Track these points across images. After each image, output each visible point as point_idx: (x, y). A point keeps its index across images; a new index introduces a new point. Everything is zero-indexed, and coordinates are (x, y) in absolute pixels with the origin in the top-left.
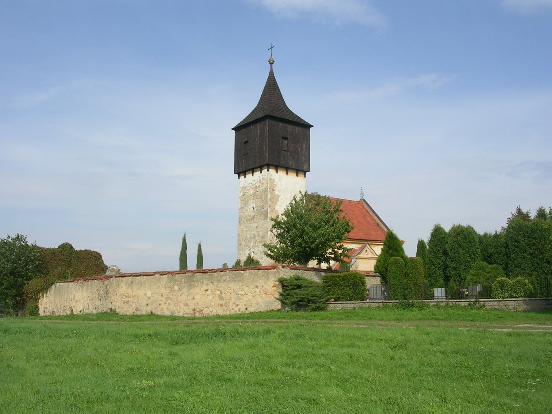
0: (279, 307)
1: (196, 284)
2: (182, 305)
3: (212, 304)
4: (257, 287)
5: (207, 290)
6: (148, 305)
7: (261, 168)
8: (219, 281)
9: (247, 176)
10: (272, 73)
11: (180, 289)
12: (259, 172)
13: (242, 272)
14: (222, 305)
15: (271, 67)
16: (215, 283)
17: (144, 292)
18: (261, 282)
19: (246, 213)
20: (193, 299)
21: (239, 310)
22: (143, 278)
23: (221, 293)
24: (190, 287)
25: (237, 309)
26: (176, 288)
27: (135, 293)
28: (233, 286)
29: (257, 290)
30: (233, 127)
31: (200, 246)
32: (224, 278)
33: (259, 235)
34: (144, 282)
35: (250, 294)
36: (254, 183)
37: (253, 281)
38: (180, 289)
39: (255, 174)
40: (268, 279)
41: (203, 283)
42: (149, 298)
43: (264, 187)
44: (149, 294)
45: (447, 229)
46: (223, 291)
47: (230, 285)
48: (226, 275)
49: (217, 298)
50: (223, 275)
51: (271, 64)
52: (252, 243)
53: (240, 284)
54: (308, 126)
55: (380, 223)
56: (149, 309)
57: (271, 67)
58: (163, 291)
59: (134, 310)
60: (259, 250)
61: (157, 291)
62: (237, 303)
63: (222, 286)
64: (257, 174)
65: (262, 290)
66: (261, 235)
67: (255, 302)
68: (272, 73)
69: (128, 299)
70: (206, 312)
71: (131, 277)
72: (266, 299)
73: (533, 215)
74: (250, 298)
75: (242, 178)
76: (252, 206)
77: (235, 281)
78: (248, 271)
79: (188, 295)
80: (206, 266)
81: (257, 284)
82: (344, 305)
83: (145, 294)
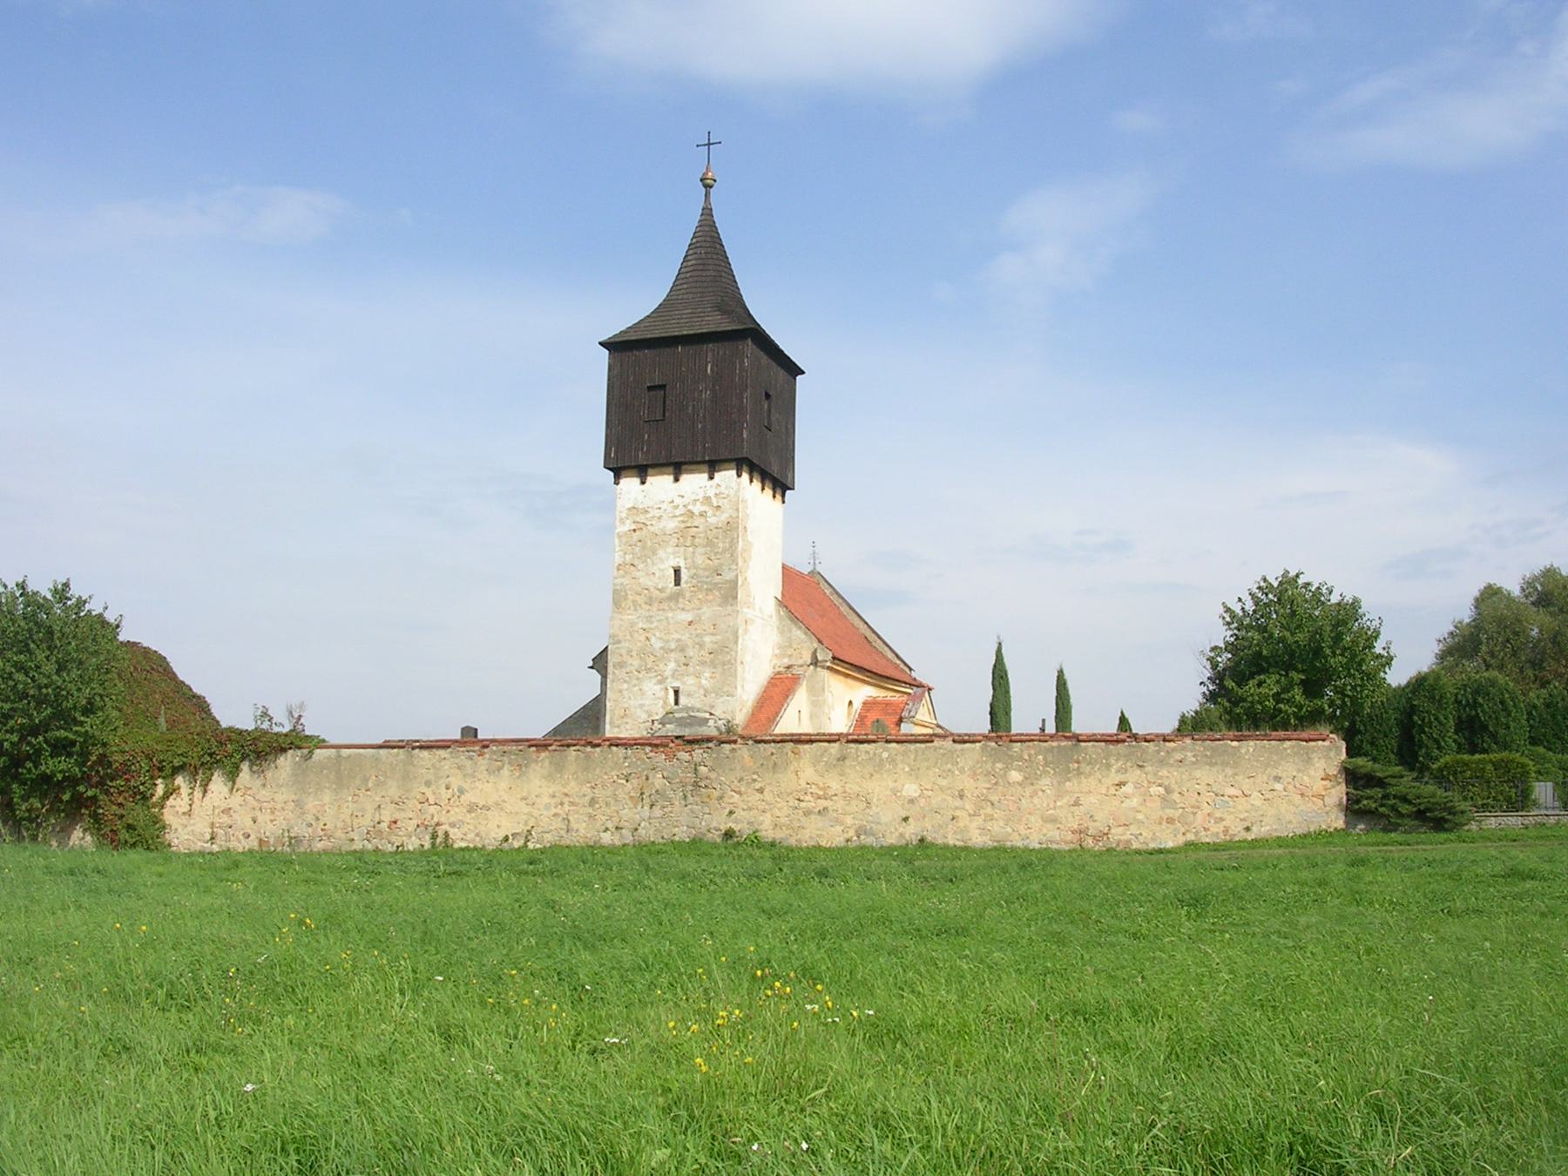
0: (1340, 823)
1: (1086, 768)
2: (1035, 821)
3: (1140, 816)
4: (1277, 779)
5: (1121, 784)
6: (906, 819)
7: (713, 466)
8: (1162, 763)
9: (649, 479)
10: (707, 212)
11: (1029, 780)
12: (706, 476)
13: (1235, 744)
14: (1170, 821)
15: (707, 195)
16: (1149, 769)
17: (891, 785)
18: (1288, 769)
19: (645, 581)
20: (1077, 804)
21: (1226, 831)
22: (885, 750)
23: (1168, 790)
24: (1065, 775)
25: (1218, 829)
26: (1015, 776)
27: (853, 788)
28: (1205, 775)
29: (1278, 786)
30: (604, 338)
31: (1000, 676)
32: (1178, 756)
33: (701, 645)
34: (892, 761)
35: (1256, 794)
36: (678, 501)
37: (1268, 765)
38: (1029, 780)
39: (685, 478)
40: (1308, 761)
41: (1108, 766)
42: (911, 801)
43: (724, 517)
44: (911, 789)
45: (123, 637)
46: (1174, 786)
47: (1198, 774)
48: (1184, 749)
49: (1157, 803)
50: (1174, 750)
51: (708, 187)
52: (672, 665)
53: (1229, 771)
54: (794, 371)
55: (872, 637)
56: (911, 832)
57: (707, 195)
58: (968, 784)
59: (851, 833)
60: (700, 686)
61: (944, 782)
62: (1218, 815)
63: (1170, 775)
64: (695, 482)
65: (1290, 787)
66: (709, 646)
67: (1272, 812)
68: (707, 212)
69: (823, 803)
70: (1118, 835)
71: (836, 745)
72: (1303, 807)
73: (1378, 648)
74: (1258, 803)
75: (630, 483)
76: (674, 562)
77: (1212, 764)
78: (1252, 743)
79: (1059, 796)
80: (1078, 726)
81: (1278, 772)
82: (1500, 820)
83: (895, 792)
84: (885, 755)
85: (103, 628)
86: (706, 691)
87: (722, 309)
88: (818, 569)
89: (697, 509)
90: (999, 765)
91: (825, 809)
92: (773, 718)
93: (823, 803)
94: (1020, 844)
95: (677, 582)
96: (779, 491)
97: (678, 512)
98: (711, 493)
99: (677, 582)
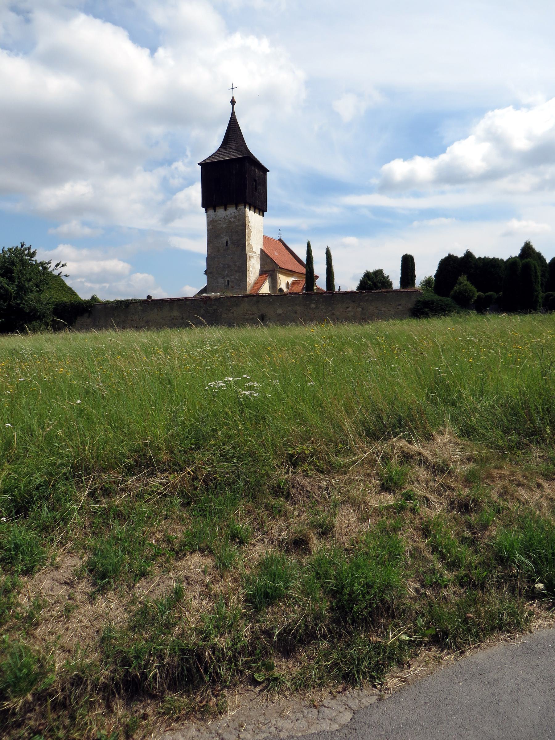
4: (400, 305)
5: (348, 308)
9: (217, 210)
10: (233, 113)
32: (367, 298)
60: (235, 279)
68: (233, 113)
69: (252, 316)
84: (271, 300)
85: (498, 259)
86: (237, 280)
87: (237, 150)
88: (281, 238)
89: (232, 220)
90: (308, 302)
91: (253, 318)
92: (259, 288)
93: (252, 316)
94: (175, 330)
95: (227, 245)
96: (261, 213)
97: (226, 221)
98: (236, 214)
99: (227, 245)
